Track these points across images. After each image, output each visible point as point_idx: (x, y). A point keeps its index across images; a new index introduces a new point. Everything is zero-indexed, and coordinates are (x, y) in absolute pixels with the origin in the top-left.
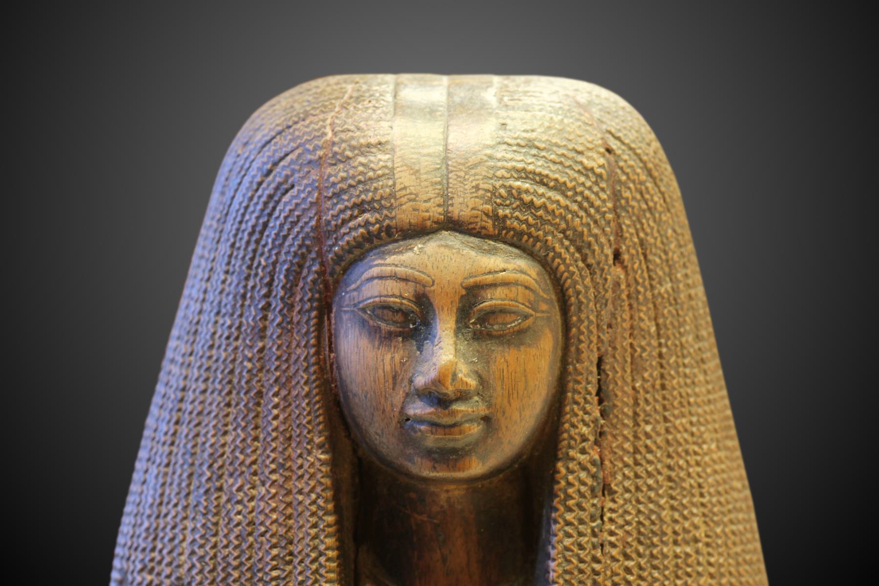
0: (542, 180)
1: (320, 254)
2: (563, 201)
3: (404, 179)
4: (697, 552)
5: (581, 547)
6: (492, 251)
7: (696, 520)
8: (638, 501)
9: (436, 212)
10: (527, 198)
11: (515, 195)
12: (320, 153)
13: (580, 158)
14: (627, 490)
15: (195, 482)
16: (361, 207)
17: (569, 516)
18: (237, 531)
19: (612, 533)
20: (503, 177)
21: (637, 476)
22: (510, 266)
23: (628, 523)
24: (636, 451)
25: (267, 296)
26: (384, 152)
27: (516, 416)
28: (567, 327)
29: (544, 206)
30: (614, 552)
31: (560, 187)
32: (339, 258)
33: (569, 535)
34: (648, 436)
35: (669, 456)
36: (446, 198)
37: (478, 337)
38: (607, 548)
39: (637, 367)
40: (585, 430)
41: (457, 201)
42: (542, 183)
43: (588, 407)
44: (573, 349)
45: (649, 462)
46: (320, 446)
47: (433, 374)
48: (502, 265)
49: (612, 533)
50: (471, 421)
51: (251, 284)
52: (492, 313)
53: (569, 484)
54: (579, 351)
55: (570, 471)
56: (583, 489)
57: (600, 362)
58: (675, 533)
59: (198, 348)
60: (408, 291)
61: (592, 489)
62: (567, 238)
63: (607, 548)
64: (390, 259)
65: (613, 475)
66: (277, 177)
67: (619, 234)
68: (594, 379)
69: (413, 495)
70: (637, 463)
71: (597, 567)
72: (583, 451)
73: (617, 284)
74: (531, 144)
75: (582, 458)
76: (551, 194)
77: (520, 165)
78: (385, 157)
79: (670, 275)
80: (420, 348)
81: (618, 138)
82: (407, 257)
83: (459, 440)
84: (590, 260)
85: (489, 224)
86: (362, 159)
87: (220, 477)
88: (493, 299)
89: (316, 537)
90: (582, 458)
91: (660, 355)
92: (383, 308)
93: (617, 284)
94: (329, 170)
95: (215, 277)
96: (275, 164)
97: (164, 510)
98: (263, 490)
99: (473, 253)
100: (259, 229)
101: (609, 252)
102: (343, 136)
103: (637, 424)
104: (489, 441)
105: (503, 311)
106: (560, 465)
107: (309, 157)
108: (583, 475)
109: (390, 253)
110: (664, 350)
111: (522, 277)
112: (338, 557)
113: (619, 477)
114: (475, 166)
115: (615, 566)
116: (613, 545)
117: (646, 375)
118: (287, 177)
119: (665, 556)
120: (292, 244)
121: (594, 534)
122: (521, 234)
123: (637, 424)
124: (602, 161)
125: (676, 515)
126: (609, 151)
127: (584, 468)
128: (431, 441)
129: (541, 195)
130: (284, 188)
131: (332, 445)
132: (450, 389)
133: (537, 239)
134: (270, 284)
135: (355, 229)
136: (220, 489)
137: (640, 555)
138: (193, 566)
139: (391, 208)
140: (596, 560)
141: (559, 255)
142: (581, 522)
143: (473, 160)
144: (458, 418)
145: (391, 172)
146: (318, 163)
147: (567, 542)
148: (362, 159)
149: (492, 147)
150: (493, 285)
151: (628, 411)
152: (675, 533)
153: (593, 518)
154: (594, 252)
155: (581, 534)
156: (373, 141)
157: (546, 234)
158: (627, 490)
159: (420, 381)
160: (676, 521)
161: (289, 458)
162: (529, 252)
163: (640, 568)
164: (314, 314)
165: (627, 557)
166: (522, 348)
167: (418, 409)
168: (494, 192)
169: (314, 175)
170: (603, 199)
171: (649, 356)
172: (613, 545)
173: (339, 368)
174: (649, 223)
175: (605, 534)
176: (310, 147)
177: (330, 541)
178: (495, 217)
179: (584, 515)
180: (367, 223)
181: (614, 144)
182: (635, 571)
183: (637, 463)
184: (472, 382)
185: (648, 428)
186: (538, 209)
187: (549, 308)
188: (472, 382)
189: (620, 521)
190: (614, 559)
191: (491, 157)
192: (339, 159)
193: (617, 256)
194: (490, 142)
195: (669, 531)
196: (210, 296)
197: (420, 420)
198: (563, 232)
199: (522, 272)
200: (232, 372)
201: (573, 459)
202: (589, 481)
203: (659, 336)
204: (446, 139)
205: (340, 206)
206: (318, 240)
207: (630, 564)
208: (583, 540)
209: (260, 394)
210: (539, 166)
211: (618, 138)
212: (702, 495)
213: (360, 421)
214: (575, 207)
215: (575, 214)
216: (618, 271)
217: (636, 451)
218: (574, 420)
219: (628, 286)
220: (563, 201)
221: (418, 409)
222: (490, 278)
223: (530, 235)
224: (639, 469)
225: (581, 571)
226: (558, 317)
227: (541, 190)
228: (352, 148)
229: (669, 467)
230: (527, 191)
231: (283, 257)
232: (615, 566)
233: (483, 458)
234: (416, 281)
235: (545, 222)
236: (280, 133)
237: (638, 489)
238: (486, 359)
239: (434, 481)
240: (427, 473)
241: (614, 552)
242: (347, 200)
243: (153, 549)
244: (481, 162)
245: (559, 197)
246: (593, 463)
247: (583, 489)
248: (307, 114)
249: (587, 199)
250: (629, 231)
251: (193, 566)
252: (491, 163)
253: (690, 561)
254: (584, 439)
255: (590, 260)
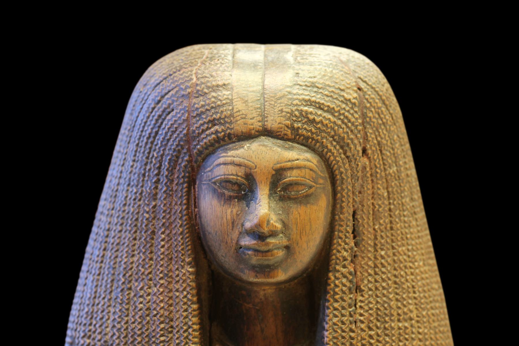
0: (320, 106)
1: (189, 150)
2: (333, 119)
3: (239, 105)
4: (412, 326)
5: (343, 323)
6: (291, 148)
7: (411, 307)
8: (377, 296)
9: (257, 125)
10: (311, 117)
11: (304, 115)
12: (189, 90)
13: (342, 93)
14: (370, 289)
15: (115, 285)
16: (213, 122)
17: (336, 305)
18: (140, 313)
19: (361, 315)
20: (297, 105)
21: (376, 281)
22: (301, 157)
23: (371, 309)
24: (376, 266)
25: (158, 174)
26: (227, 90)
27: (305, 246)
28: (335, 193)
29: (321, 122)
30: (363, 326)
31: (331, 111)
32: (200, 153)
33: (336, 316)
34: (382, 257)
35: (395, 269)
36: (263, 117)
37: (282, 199)
38: (359, 324)
39: (376, 217)
40: (345, 254)
41: (270, 118)
42: (320, 108)
43: (347, 240)
44: (338, 206)
45: (383, 273)
46: (189, 263)
47: (256, 221)
48: (297, 157)
49: (361, 315)
50: (278, 248)
51: (148, 167)
52: (291, 185)
53: (336, 286)
54: (342, 207)
55: (337, 278)
56: (344, 289)
57: (354, 214)
58: (399, 315)
59: (117, 206)
60: (241, 172)
61: (350, 289)
62: (334, 140)
63: (359, 324)
64: (230, 153)
65: (362, 280)
66: (163, 105)
67: (366, 138)
68: (351, 224)
69: (244, 292)
70: (376, 273)
71: (352, 335)
72: (344, 267)
73: (364, 168)
74: (313, 85)
75: (344, 270)
76: (325, 114)
77: (307, 98)
78: (228, 93)
79: (396, 162)
80: (248, 206)
81: (365, 82)
82: (240, 152)
83: (271, 260)
84: (349, 154)
85: (289, 132)
86: (214, 94)
87: (130, 282)
88: (291, 176)
89: (186, 317)
90: (344, 270)
91: (390, 210)
92: (226, 182)
93: (364, 168)
94: (194, 100)
95: (127, 164)
96: (163, 97)
97: (97, 301)
98: (155, 290)
99: (279, 150)
100: (153, 135)
101: (360, 149)
102: (203, 80)
103: (376, 250)
104: (289, 260)
105: (297, 184)
106: (331, 275)
107: (183, 93)
108: (344, 280)
109: (230, 149)
110: (392, 207)
111: (308, 164)
112: (200, 329)
113: (366, 282)
114: (281, 98)
115: (363, 334)
116: (362, 322)
117: (381, 221)
118: (170, 105)
119: (393, 328)
120: (172, 144)
121: (351, 316)
122: (307, 138)
123: (376, 250)
124: (355, 95)
125: (399, 304)
126: (360, 89)
127: (345, 277)
128: (255, 260)
129: (320, 115)
130: (168, 111)
131: (196, 263)
132: (266, 230)
133: (317, 141)
134: (159, 168)
135: (210, 135)
136: (130, 289)
137: (378, 328)
138: (114, 334)
139: (231, 123)
140: (352, 331)
141: (330, 151)
142: (343, 308)
143: (279, 94)
144: (271, 247)
145: (231, 102)
146: (188, 96)
147: (335, 320)
148: (214, 94)
149: (290, 87)
150: (291, 168)
151: (371, 242)
152: (399, 315)
153: (350, 306)
154: (350, 149)
155: (343, 315)
156: (220, 83)
157: (322, 138)
158: (370, 289)
159: (248, 225)
160: (399, 308)
161: (171, 270)
162: (312, 149)
163: (378, 335)
164: (185, 185)
165: (370, 329)
166: (308, 206)
167: (247, 241)
168: (292, 113)
169: (186, 104)
170: (356, 118)
171: (383, 210)
172: (362, 322)
173: (200, 217)
174: (383, 131)
175: (358, 316)
176: (183, 87)
177: (195, 320)
178: (293, 128)
179: (345, 304)
180: (217, 132)
181: (363, 85)
182: (375, 337)
183: (376, 273)
184: (279, 226)
185: (383, 253)
186: (318, 123)
187: (324, 182)
188: (279, 226)
189: (366, 308)
190: (362, 330)
191: (290, 93)
192: (200, 94)
193: (364, 151)
194: (289, 84)
195: (395, 314)
196: (124, 175)
197: (248, 248)
198: (333, 137)
199: (308, 160)
200: (137, 220)
201: (338, 271)
202: (348, 284)
203: (389, 198)
204: (263, 82)
205: (201, 122)
206: (188, 142)
207: (372, 333)
208: (345, 319)
209: (153, 232)
210: (318, 98)
211: (365, 82)
212: (414, 292)
213: (213, 248)
214: (339, 122)
215: (340, 127)
216: (365, 160)
217: (376, 266)
218: (339, 248)
219: (371, 169)
220: (333, 119)
221: (247, 241)
222: (289, 164)
223: (313, 139)
224: (377, 277)
225: (343, 337)
226: (329, 187)
227: (320, 112)
228: (208, 88)
229: (395, 276)
230: (311, 113)
231: (167, 152)
232: (363, 334)
233: (285, 271)
234: (246, 166)
235: (322, 131)
236: (165, 78)
237: (377, 288)
238: (287, 212)
239: (256, 284)
240: (252, 279)
241: (363, 326)
242: (205, 118)
243: (90, 324)
244: (284, 96)
245: (330, 116)
246: (350, 273)
247: (344, 289)
248: (181, 68)
249: (347, 117)
250: (371, 136)
251: (114, 334)
252: (290, 96)
253: (407, 331)
254: (345, 259)
255: (349, 154)
